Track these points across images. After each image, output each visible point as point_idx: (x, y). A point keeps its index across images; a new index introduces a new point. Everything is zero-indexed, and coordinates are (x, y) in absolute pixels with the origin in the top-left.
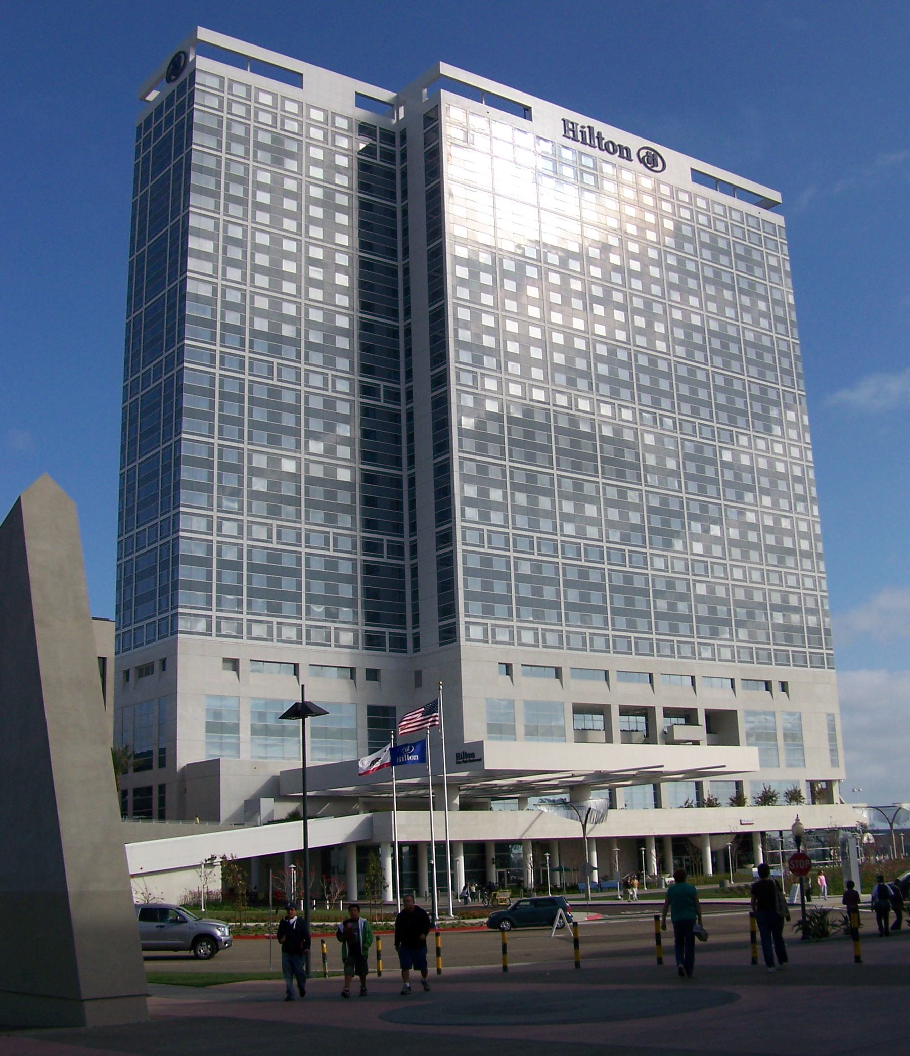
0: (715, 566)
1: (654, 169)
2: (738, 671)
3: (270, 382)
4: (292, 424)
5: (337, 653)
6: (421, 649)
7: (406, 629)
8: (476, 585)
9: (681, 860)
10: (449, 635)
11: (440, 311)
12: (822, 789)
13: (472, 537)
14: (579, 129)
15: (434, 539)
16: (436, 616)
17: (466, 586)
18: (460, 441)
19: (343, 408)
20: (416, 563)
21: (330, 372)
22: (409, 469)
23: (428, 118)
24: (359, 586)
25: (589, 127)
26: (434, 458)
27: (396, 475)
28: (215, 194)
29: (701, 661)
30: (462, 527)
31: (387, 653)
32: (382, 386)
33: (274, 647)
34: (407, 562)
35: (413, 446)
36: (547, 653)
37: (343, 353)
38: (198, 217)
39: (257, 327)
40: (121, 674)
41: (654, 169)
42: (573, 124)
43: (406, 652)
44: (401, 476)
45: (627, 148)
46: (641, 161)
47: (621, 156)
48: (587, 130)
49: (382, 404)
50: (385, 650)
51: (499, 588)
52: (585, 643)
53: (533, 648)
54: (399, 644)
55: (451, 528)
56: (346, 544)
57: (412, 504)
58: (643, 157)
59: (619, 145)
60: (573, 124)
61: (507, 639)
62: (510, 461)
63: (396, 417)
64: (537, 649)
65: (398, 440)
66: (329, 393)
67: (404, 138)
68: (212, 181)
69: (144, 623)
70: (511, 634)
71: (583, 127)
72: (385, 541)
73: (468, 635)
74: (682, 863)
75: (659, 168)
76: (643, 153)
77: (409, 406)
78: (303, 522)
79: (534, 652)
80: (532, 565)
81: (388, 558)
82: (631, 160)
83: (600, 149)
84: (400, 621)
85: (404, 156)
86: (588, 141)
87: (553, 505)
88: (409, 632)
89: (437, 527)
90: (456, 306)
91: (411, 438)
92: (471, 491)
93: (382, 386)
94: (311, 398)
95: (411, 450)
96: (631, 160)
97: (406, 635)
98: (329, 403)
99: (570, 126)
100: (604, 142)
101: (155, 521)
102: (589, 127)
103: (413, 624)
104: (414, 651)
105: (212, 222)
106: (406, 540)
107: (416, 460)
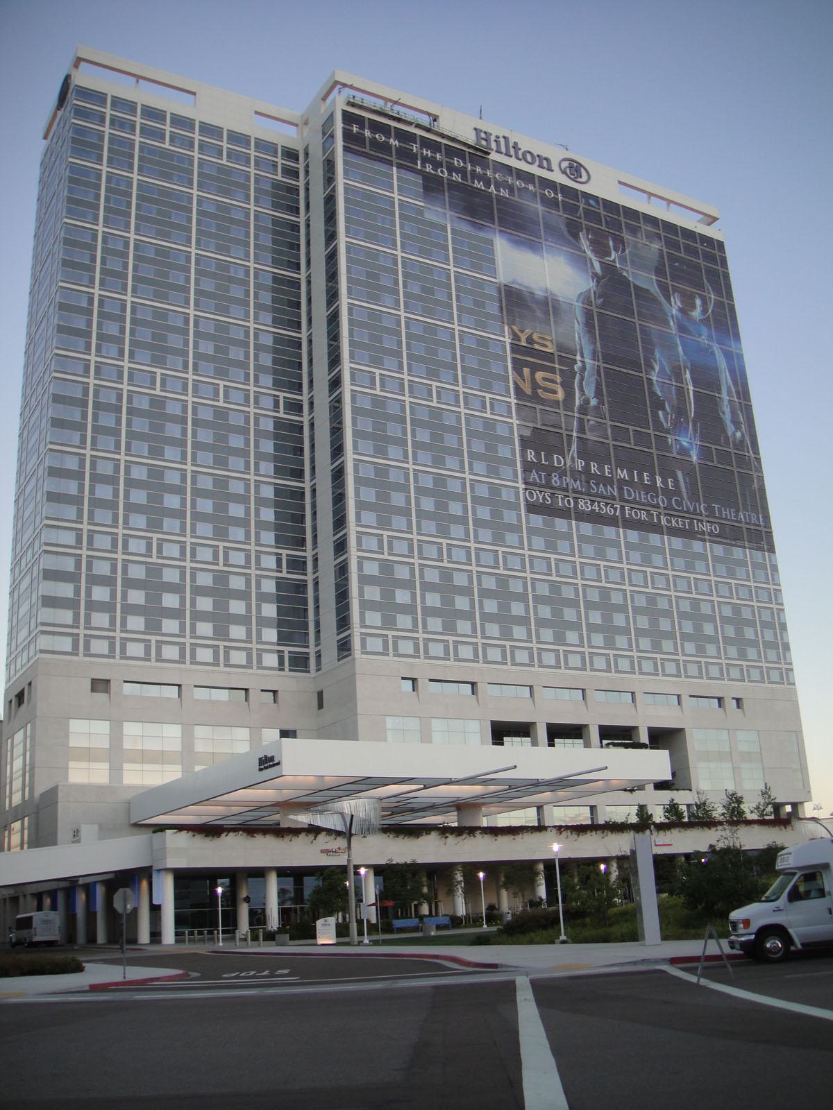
0: (656, 577)
1: (579, 180)
2: (685, 686)
3: (227, 383)
5: (293, 677)
14: (493, 138)
15: (332, 548)
25: (504, 137)
29: (641, 677)
30: (358, 532)
33: (151, 667)
36: (460, 667)
40: (8, 704)
41: (579, 180)
42: (485, 133)
43: (309, 672)
45: (546, 159)
47: (541, 166)
48: (502, 141)
51: (665, 625)
52: (584, 663)
53: (381, 657)
59: (538, 156)
60: (485, 133)
61: (411, 652)
64: (505, 667)
75: (584, 178)
80: (380, 565)
82: (552, 171)
96: (552, 171)
99: (483, 135)
102: (504, 137)
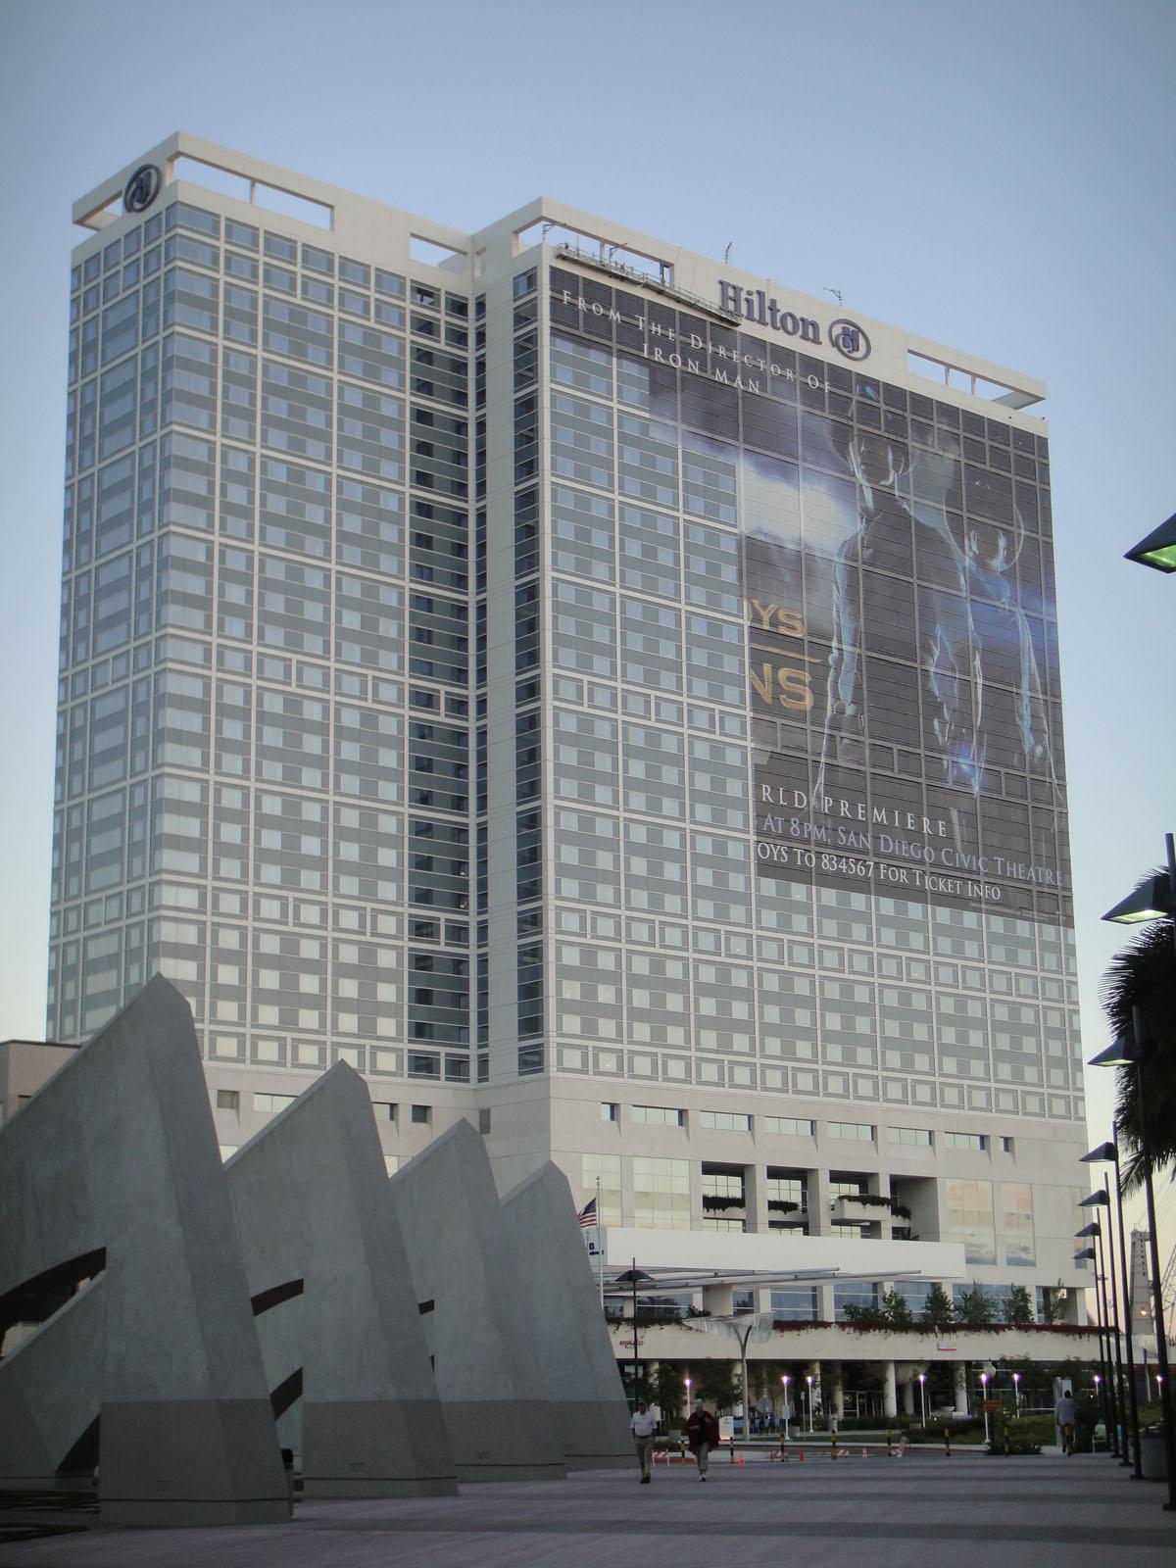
4: (320, 520)
6: (487, 495)
7: (467, 947)
8: (569, 627)
9: (853, 1395)
10: (532, 1061)
11: (533, 588)
12: (1062, 1300)
13: (568, 690)
14: (744, 295)
16: (513, 701)
17: (555, 625)
18: (554, 555)
19: (389, 598)
20: (486, 921)
21: (371, 673)
22: (478, 501)
23: (521, 317)
24: (406, 1020)
25: (759, 293)
26: (516, 484)
27: (459, 356)
28: (205, 503)
31: (442, 1082)
32: (442, 693)
34: (472, 952)
35: (484, 560)
37: (390, 1010)
38: (179, 677)
39: (264, 844)
42: (734, 288)
43: (467, 1081)
44: (467, 825)
46: (835, 344)
47: (804, 337)
48: (755, 298)
49: (442, 718)
50: (438, 1078)
54: (458, 1068)
55: (538, 676)
56: (388, 692)
57: (482, 548)
58: (837, 337)
59: (803, 320)
62: (620, 494)
63: (461, 736)
65: (462, 643)
66: (369, 704)
67: (481, 307)
68: (205, 381)
69: (123, 295)
70: (620, 1060)
71: (749, 293)
72: (443, 1055)
73: (559, 1025)
74: (854, 1401)
76: (837, 330)
77: (481, 412)
78: (332, 692)
79: (652, 1088)
81: (446, 716)
82: (819, 343)
83: (774, 327)
84: (459, 901)
85: (481, 337)
86: (756, 316)
87: (684, 875)
88: (473, 1052)
89: (519, 904)
90: (561, 1047)
91: (482, 548)
92: (572, 990)
93: (442, 693)
94: (346, 581)
95: (481, 566)
96: (819, 343)
97: (468, 1056)
98: (369, 718)
99: (731, 293)
100: (779, 315)
101: (132, 353)
102: (759, 293)
103: (479, 1040)
104: (480, 1081)
105: (199, 683)
106: (471, 693)
107: (491, 901)
